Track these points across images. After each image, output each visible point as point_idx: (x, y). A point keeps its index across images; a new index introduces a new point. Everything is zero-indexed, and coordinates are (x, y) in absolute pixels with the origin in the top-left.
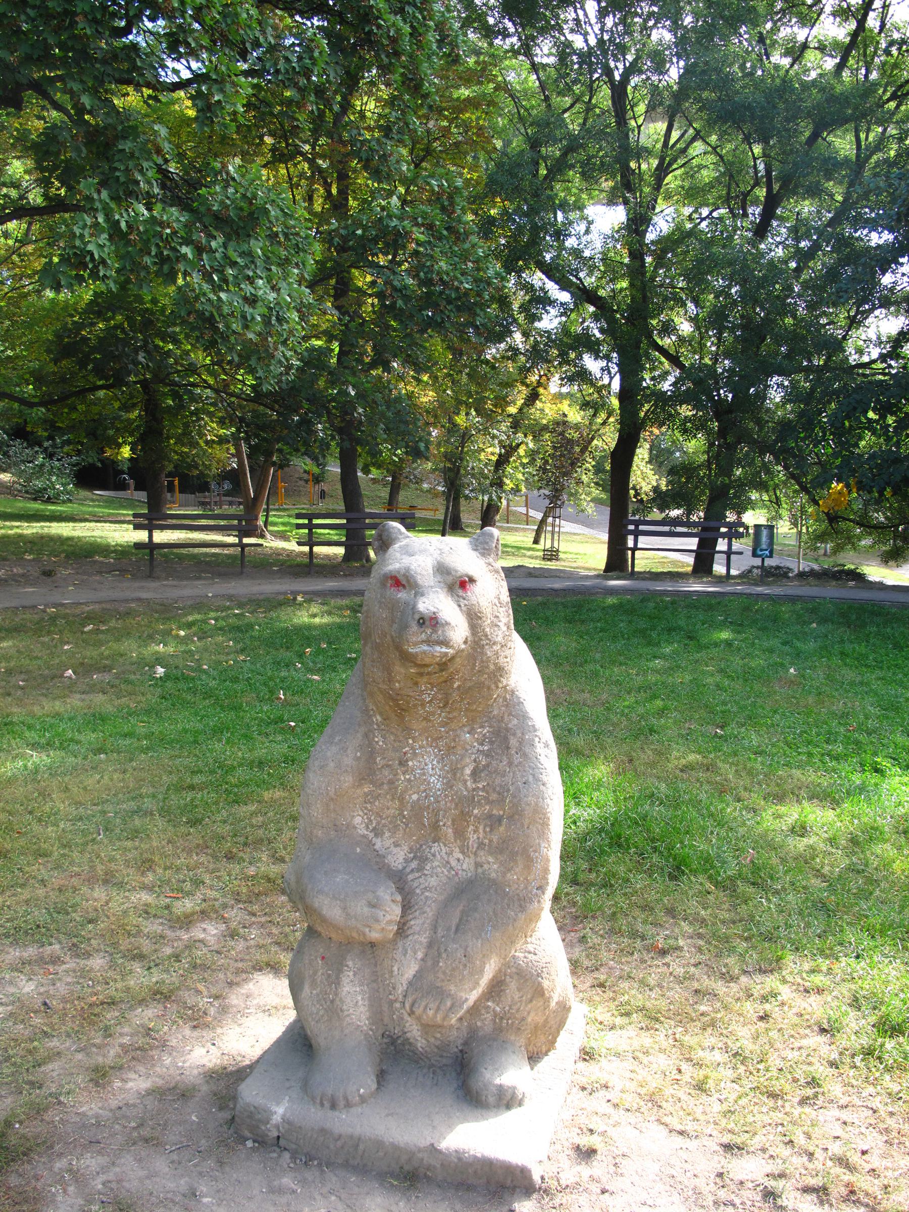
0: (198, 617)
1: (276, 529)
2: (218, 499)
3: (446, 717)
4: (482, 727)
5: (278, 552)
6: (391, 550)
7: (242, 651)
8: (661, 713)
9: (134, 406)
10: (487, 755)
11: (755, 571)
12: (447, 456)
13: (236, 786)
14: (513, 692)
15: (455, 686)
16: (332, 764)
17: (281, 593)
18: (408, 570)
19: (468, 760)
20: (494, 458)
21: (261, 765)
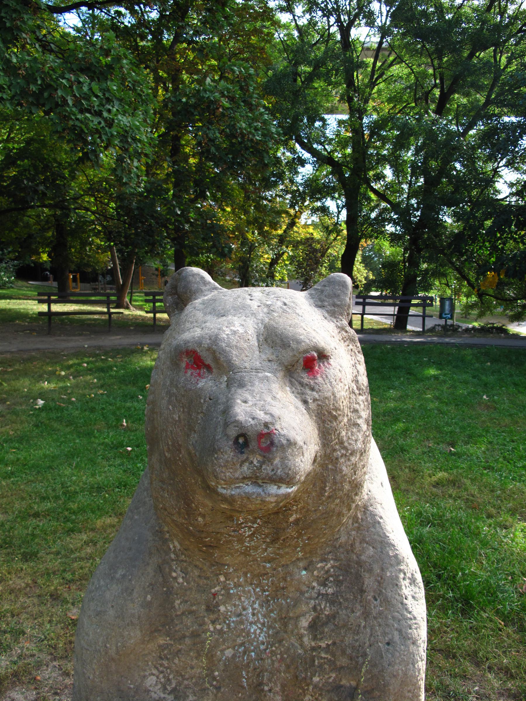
0: (76, 361)
1: (137, 303)
2: (103, 286)
3: (274, 553)
4: (324, 560)
5: (136, 318)
6: (189, 308)
7: (102, 387)
8: (405, 432)
9: (49, 228)
10: (332, 600)
11: (437, 327)
12: (241, 259)
13: (74, 513)
14: (365, 507)
15: (291, 519)
16: (111, 612)
17: (133, 345)
18: (215, 339)
19: (304, 608)
20: (269, 261)
21: (99, 489)
